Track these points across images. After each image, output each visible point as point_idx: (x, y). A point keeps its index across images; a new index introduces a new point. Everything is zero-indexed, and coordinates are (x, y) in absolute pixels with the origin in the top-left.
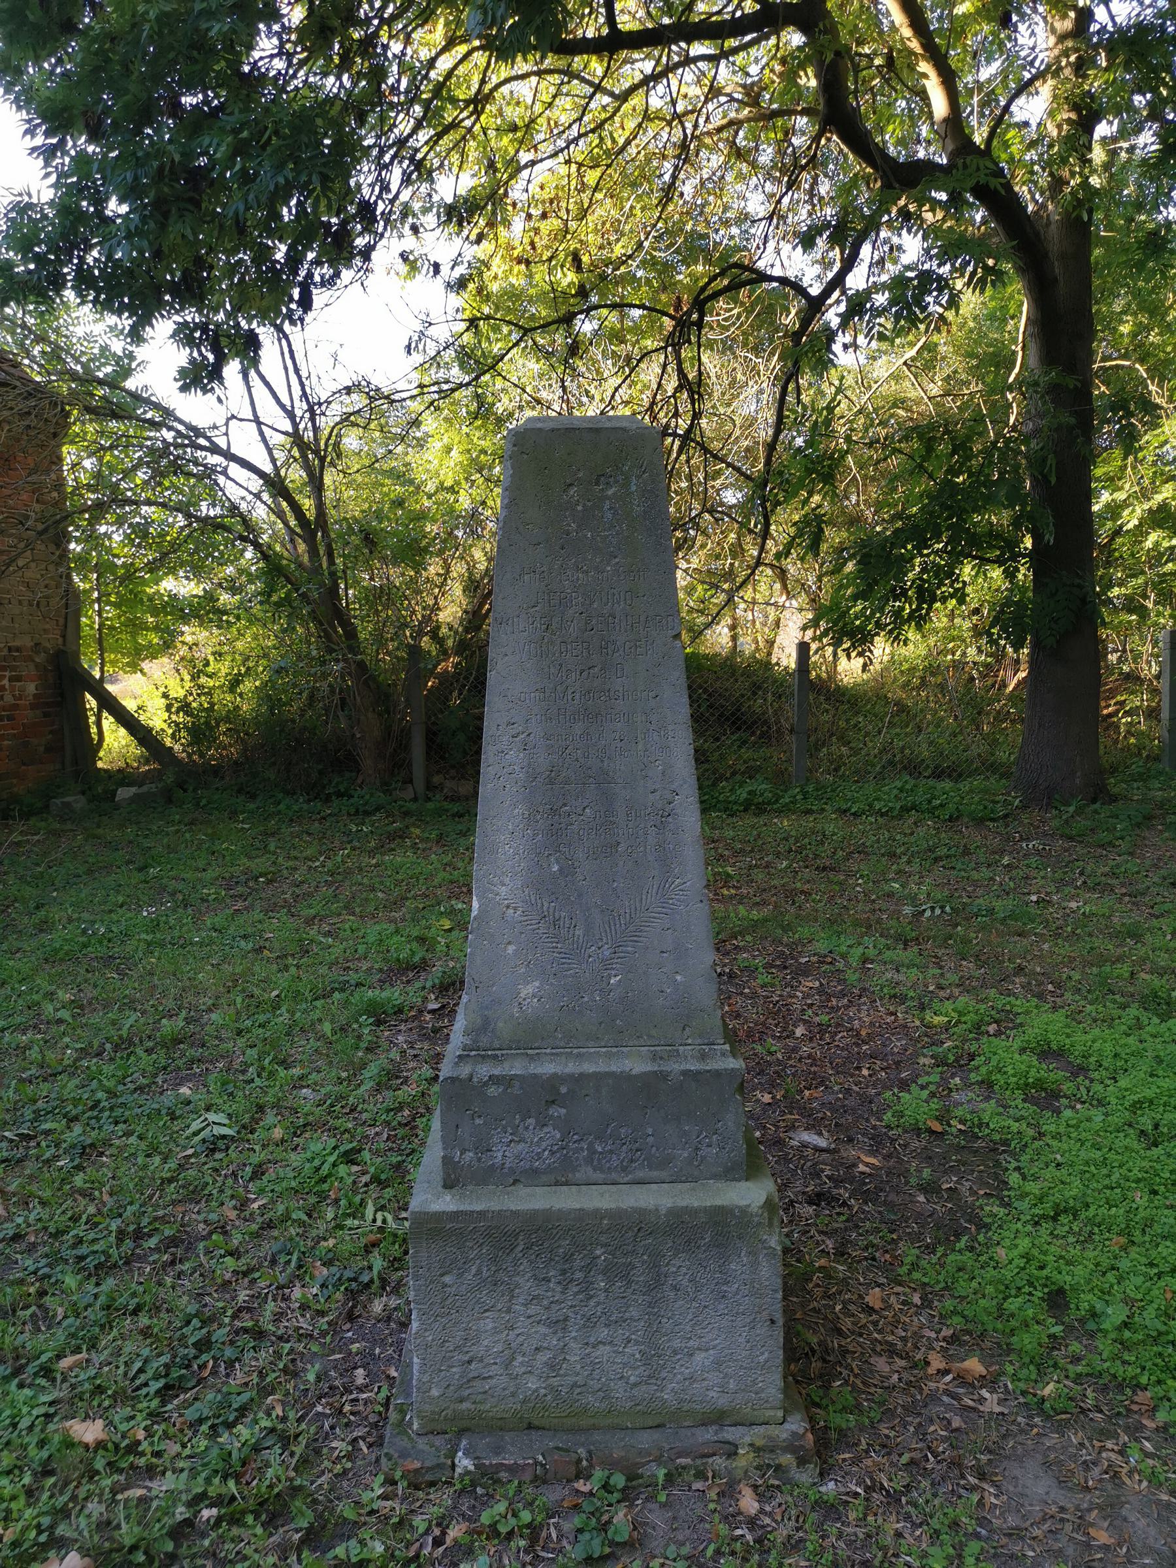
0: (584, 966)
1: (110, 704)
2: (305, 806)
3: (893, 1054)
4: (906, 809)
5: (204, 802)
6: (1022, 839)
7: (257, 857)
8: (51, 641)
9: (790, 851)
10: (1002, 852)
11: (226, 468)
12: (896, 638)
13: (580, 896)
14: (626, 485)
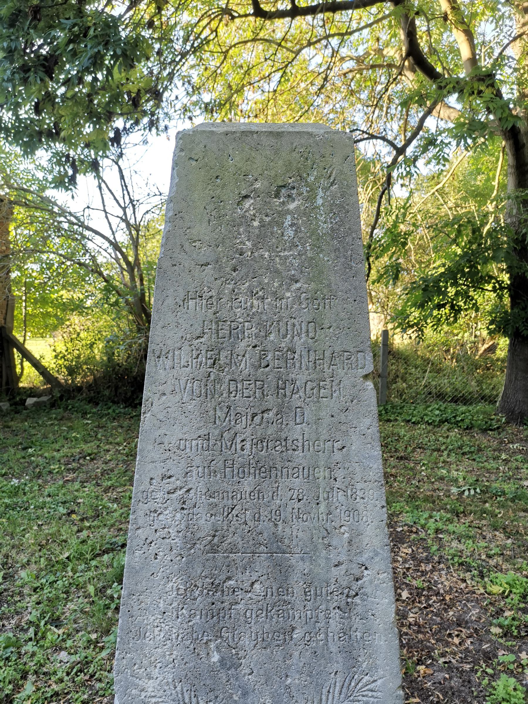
1: (26, 355)
2: (122, 411)
3: (472, 622)
4: (442, 422)
5: (70, 407)
6: (509, 443)
7: (91, 442)
10: (500, 450)
12: (435, 329)
14: (311, 198)
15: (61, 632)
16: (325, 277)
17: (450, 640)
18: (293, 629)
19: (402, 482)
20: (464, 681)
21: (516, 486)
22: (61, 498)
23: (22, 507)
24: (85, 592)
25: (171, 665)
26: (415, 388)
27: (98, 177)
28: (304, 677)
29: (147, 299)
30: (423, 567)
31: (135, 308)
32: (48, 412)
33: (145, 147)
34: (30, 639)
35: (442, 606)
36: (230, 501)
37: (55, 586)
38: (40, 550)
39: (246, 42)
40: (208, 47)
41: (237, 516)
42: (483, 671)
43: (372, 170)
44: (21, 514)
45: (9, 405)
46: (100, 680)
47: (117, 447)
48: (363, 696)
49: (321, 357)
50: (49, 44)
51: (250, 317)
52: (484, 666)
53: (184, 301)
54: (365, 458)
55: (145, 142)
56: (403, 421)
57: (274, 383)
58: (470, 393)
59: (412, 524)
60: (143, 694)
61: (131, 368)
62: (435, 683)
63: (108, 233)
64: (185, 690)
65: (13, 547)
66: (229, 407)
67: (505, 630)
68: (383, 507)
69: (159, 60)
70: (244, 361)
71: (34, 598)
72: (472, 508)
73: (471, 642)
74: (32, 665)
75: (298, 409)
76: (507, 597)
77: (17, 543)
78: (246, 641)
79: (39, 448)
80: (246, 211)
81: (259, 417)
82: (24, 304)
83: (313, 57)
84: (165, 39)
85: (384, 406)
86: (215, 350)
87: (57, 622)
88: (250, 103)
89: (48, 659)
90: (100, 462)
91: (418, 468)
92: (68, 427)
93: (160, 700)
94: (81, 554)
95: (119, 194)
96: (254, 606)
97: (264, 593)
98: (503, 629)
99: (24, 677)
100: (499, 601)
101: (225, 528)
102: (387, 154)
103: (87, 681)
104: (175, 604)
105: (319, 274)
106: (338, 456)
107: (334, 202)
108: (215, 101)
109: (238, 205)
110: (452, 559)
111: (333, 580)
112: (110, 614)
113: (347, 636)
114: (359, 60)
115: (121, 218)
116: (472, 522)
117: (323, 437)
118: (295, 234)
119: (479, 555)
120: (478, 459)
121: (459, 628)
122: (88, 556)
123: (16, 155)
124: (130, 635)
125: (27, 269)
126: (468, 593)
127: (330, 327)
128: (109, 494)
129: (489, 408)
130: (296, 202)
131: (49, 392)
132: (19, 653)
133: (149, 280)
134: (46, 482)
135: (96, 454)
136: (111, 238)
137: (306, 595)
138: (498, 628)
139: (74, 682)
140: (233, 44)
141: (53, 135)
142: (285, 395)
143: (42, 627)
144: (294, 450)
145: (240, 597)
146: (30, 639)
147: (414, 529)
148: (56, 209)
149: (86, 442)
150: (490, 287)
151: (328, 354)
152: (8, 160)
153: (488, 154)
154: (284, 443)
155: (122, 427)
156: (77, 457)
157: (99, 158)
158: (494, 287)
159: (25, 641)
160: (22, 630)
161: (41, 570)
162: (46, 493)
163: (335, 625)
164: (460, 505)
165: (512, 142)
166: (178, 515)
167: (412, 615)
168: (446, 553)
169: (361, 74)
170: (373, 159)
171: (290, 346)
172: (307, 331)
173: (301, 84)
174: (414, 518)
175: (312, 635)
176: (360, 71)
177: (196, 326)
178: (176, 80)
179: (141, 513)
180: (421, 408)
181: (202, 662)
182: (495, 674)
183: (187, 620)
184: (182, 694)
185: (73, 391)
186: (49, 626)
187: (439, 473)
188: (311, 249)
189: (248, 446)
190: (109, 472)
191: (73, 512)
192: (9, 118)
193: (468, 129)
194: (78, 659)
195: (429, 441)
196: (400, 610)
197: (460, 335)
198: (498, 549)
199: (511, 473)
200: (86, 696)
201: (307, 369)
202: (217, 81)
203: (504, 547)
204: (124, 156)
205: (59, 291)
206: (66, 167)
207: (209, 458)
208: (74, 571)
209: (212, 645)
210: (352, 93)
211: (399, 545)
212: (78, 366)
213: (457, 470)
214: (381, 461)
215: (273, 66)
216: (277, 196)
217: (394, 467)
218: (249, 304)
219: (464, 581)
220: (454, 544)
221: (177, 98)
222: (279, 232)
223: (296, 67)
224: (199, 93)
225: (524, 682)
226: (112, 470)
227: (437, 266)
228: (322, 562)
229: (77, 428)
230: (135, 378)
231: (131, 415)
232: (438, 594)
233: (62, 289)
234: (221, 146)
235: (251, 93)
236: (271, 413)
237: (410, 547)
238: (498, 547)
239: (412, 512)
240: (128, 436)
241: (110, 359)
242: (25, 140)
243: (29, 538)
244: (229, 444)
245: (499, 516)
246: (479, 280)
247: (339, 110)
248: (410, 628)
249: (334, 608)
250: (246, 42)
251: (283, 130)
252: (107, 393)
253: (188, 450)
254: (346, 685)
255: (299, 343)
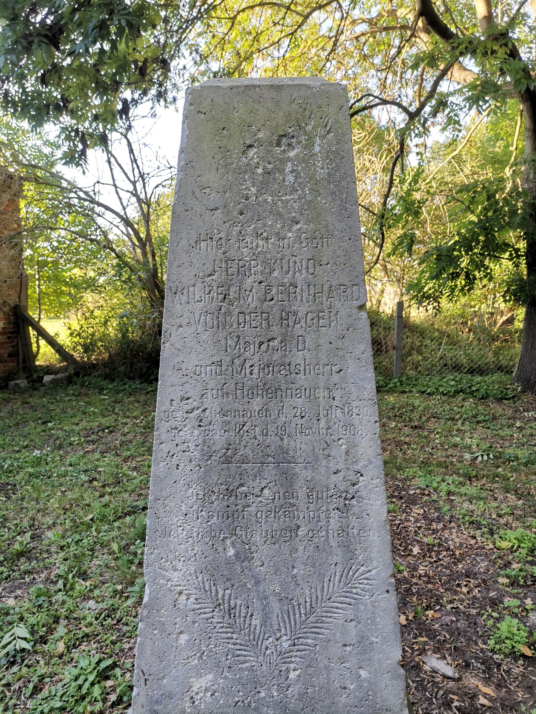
0: (261, 658)
1: (42, 333)
2: (139, 386)
3: (480, 573)
4: (457, 392)
5: (87, 383)
6: (524, 411)
7: (108, 416)
8: (13, 300)
9: (396, 416)
10: (514, 419)
11: (103, 214)
12: (451, 300)
13: (257, 583)
14: (309, 145)
15: (88, 584)
16: (322, 218)
17: (459, 589)
18: (298, 527)
19: (416, 449)
20: (470, 623)
21: (529, 452)
22: (82, 467)
23: (45, 476)
24: (110, 549)
25: (193, 559)
26: (430, 360)
27: (108, 152)
28: (308, 568)
29: (159, 275)
30: (434, 526)
31: (148, 284)
32: (65, 389)
33: (153, 120)
34: (60, 590)
35: (452, 560)
36: (241, 419)
37: (81, 544)
38: (65, 513)
39: (252, 7)
40: (215, 13)
41: (247, 432)
42: (489, 615)
43: (387, 138)
44: (44, 482)
45: (26, 382)
46: (127, 624)
47: (134, 421)
48: (360, 584)
49: (320, 290)
50: (52, 14)
51: (255, 256)
52: (490, 610)
53: (196, 242)
54: (361, 380)
55: (154, 115)
56: (418, 392)
57: (278, 315)
58: (486, 364)
59: (425, 487)
60: (170, 583)
61: (146, 345)
62: (442, 625)
63: (118, 209)
64: (205, 579)
65: (39, 511)
66: (238, 337)
67: (512, 580)
68: (376, 422)
69: (166, 29)
70: (251, 296)
71: (62, 555)
72: (485, 472)
73: (479, 591)
74: (63, 612)
75: (300, 338)
76: (515, 551)
77: (42, 507)
78: (257, 538)
79: (59, 422)
80: (250, 160)
81: (265, 345)
82: (37, 283)
83: (324, 21)
84: (171, 6)
85: (399, 377)
86: (225, 286)
87: (84, 575)
88: (259, 71)
89: (78, 606)
90: (119, 435)
91: (432, 436)
92: (85, 403)
93: (184, 588)
94: (104, 516)
95: (128, 168)
96: (264, 508)
97: (273, 497)
98: (510, 580)
99: (57, 621)
100: (508, 555)
101: (237, 442)
102: (400, 119)
103: (115, 625)
104: (195, 507)
105: (317, 215)
106: (336, 378)
107: (330, 149)
108: (224, 70)
109: (243, 154)
110: (463, 518)
111: (332, 486)
112: (133, 568)
113: (345, 533)
114: (370, 22)
115: (132, 193)
116: (484, 485)
117: (322, 362)
118: (295, 180)
119: (490, 515)
120: (492, 427)
121: (468, 579)
122: (111, 518)
123: (23, 131)
124: (157, 533)
125: (39, 247)
126: (477, 549)
127: (328, 263)
128: (129, 463)
129: (505, 378)
130: (296, 150)
131: (66, 369)
132: (51, 603)
133: (161, 256)
134: (67, 453)
135: (114, 427)
136: (122, 213)
137: (309, 498)
138: (505, 578)
139: (102, 625)
140: (241, 9)
141: (61, 107)
142: (288, 326)
143: (70, 580)
144: (296, 373)
145: (251, 501)
146: (60, 590)
147: (427, 492)
148: (65, 184)
149: (104, 416)
150: (507, 255)
151: (326, 288)
152: (15, 137)
153: (508, 119)
154: (287, 368)
155: (138, 402)
156: (96, 430)
157: (107, 132)
158: (511, 255)
159: (55, 592)
160: (52, 582)
161: (66, 530)
162: (68, 463)
163: (334, 524)
164: (473, 470)
165: (529, 103)
166: (196, 432)
167: (422, 568)
168: (457, 512)
169: (375, 38)
170: (388, 127)
171: (292, 281)
172: (307, 268)
173: (312, 50)
174: (427, 482)
175: (314, 532)
176: (373, 34)
177: (208, 265)
178: (182, 47)
179: (163, 430)
180: (436, 379)
181: (220, 556)
182: (500, 617)
183: (206, 521)
184: (203, 583)
185: (89, 367)
186: (77, 579)
187: (453, 441)
188: (310, 193)
189: (256, 371)
190: (128, 443)
191: (94, 479)
192: (16, 92)
193: (482, 92)
194: (106, 607)
195: (444, 411)
196: (411, 563)
197: (477, 307)
198: (509, 509)
199: (525, 440)
200: (114, 638)
201: (308, 302)
202: (225, 48)
203: (516, 507)
204: (132, 129)
205: (72, 269)
206: (76, 142)
207: (222, 381)
208: (98, 531)
209: (228, 542)
210: (365, 57)
211: (411, 506)
212: (93, 344)
213: (471, 438)
214: (374, 382)
215: (282, 32)
216: (278, 144)
217: (408, 436)
218: (254, 244)
219: (474, 537)
220: (466, 505)
221: (185, 67)
222: (281, 177)
223: (307, 32)
224: (207, 62)
225: (528, 624)
226: (131, 442)
227: (451, 233)
228: (323, 470)
229: (95, 403)
230: (150, 355)
231: (147, 390)
232: (448, 549)
233: (75, 267)
234: (227, 100)
235: (260, 60)
236: (276, 342)
237: (422, 508)
238: (508, 507)
239: (425, 476)
240: (145, 410)
241: (123, 336)
242: (32, 113)
243: (53, 503)
244: (239, 369)
245: (512, 479)
246: (494, 248)
247: (352, 76)
248: (420, 579)
249: (334, 509)
250: (252, 7)
251: (283, 83)
252: (122, 369)
253: (203, 375)
254: (345, 574)
255: (300, 278)
